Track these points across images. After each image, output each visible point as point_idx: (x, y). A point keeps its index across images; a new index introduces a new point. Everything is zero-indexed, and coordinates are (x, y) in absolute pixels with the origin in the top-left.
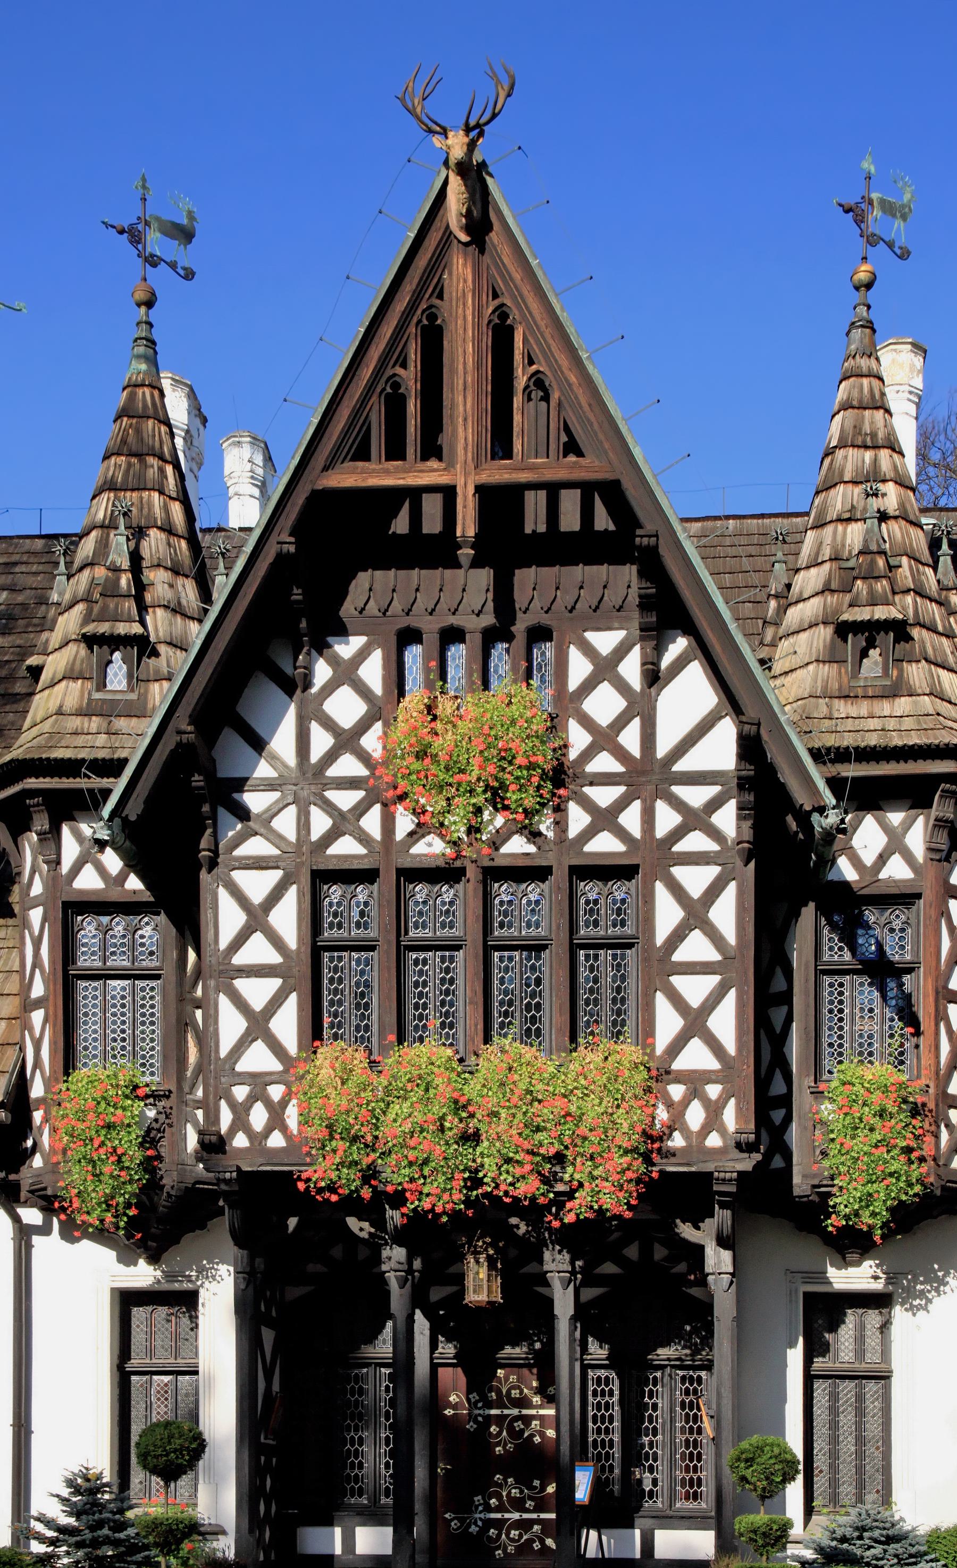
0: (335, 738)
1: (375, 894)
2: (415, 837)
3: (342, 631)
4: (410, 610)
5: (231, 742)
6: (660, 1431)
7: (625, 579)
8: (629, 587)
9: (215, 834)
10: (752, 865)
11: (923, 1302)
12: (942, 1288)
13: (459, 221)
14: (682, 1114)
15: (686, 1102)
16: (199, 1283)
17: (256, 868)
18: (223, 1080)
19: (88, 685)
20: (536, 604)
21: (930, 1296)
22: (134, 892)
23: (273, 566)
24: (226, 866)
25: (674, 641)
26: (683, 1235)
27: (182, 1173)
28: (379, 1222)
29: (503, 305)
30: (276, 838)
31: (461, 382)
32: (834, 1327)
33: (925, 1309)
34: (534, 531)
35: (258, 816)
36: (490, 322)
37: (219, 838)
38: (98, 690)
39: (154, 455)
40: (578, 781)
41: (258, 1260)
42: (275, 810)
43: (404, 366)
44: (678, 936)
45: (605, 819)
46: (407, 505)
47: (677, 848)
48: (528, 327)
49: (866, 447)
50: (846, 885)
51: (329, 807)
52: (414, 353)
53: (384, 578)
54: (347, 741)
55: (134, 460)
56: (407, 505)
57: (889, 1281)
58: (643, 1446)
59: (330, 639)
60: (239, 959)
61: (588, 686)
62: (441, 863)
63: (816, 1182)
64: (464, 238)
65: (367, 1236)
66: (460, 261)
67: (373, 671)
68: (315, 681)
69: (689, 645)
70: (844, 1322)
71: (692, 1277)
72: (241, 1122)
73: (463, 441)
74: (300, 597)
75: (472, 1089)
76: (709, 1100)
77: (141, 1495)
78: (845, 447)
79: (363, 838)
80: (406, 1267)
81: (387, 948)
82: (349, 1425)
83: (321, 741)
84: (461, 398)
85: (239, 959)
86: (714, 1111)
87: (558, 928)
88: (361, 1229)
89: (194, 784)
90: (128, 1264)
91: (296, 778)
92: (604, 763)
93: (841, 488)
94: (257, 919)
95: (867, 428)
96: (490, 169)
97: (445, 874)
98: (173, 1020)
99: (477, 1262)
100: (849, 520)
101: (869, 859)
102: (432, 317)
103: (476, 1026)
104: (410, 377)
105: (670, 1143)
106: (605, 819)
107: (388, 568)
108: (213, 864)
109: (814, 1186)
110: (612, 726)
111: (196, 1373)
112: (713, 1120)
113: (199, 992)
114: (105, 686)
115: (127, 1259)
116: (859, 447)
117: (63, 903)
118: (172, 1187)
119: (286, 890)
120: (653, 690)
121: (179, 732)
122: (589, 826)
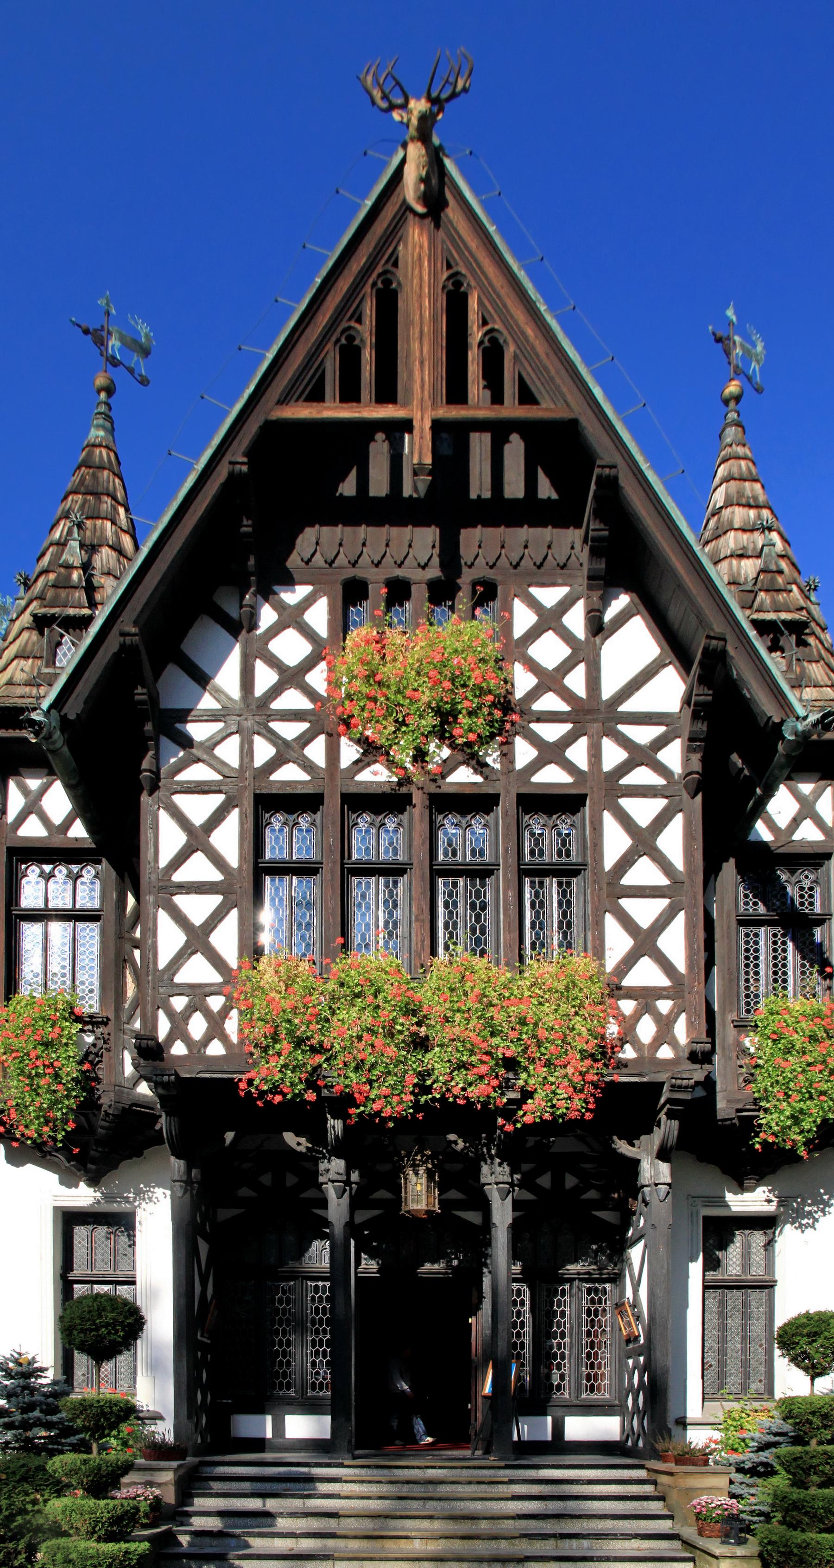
0: (280, 674)
1: (318, 822)
2: (361, 764)
3: (289, 581)
4: (356, 562)
5: (173, 674)
6: (567, 1334)
7: (570, 542)
8: (572, 548)
9: (157, 757)
10: (699, 797)
11: (811, 1221)
12: (827, 1209)
13: (417, 189)
14: (633, 1027)
15: (637, 1017)
16: (137, 1203)
17: (198, 792)
18: (161, 990)
19: (39, 662)
20: (481, 561)
21: (816, 1216)
22: (76, 839)
23: (225, 486)
24: (168, 790)
25: (617, 598)
26: (620, 1151)
27: (119, 1094)
28: (317, 1134)
29: (458, 273)
30: (218, 765)
31: (417, 331)
32: (724, 1245)
33: (813, 1227)
34: (479, 497)
35: (201, 744)
36: (444, 287)
37: (161, 761)
38: (47, 666)
39: (108, 495)
40: (525, 717)
41: (194, 1172)
42: (218, 738)
43: (359, 321)
44: (626, 862)
45: (552, 753)
46: (354, 472)
47: (624, 781)
48: (483, 290)
49: (750, 506)
50: (764, 845)
51: (273, 737)
52: (369, 310)
53: (331, 534)
54: (292, 677)
55: (90, 498)
56: (354, 472)
57: (780, 1204)
58: (551, 1347)
59: (276, 588)
60: (179, 876)
61: (533, 634)
62: (387, 789)
63: (740, 1106)
64: (420, 209)
65: (304, 1150)
66: (417, 231)
67: (319, 616)
68: (260, 624)
69: (632, 601)
70: (733, 1242)
71: (616, 1196)
72: (179, 1030)
73: (419, 381)
74: (250, 529)
75: (425, 994)
76: (660, 1014)
77: (84, 1385)
78: (731, 505)
79: (307, 766)
80: (344, 1178)
81: (331, 870)
82: (277, 1330)
83: (265, 677)
84: (417, 345)
85: (179, 876)
86: (665, 1025)
87: (506, 850)
88: (299, 1144)
89: (137, 697)
90: (69, 1186)
91: (241, 709)
92: (550, 702)
93: (731, 534)
94: (198, 839)
95: (748, 493)
96: (446, 152)
97: (387, 803)
98: (112, 955)
99: (417, 1174)
100: (741, 556)
101: (783, 822)
102: (387, 283)
103: (423, 941)
104: (366, 332)
105: (621, 1055)
106: (552, 753)
107: (336, 525)
108: (154, 787)
109: (738, 1111)
110: (274, 744)
111: (133, 1283)
112: (664, 1034)
113: (138, 934)
114: (54, 663)
115: (68, 1181)
116: (744, 506)
117: (8, 848)
118: (110, 1106)
119: (229, 812)
120: (598, 639)
121: (123, 634)
122: (536, 759)
